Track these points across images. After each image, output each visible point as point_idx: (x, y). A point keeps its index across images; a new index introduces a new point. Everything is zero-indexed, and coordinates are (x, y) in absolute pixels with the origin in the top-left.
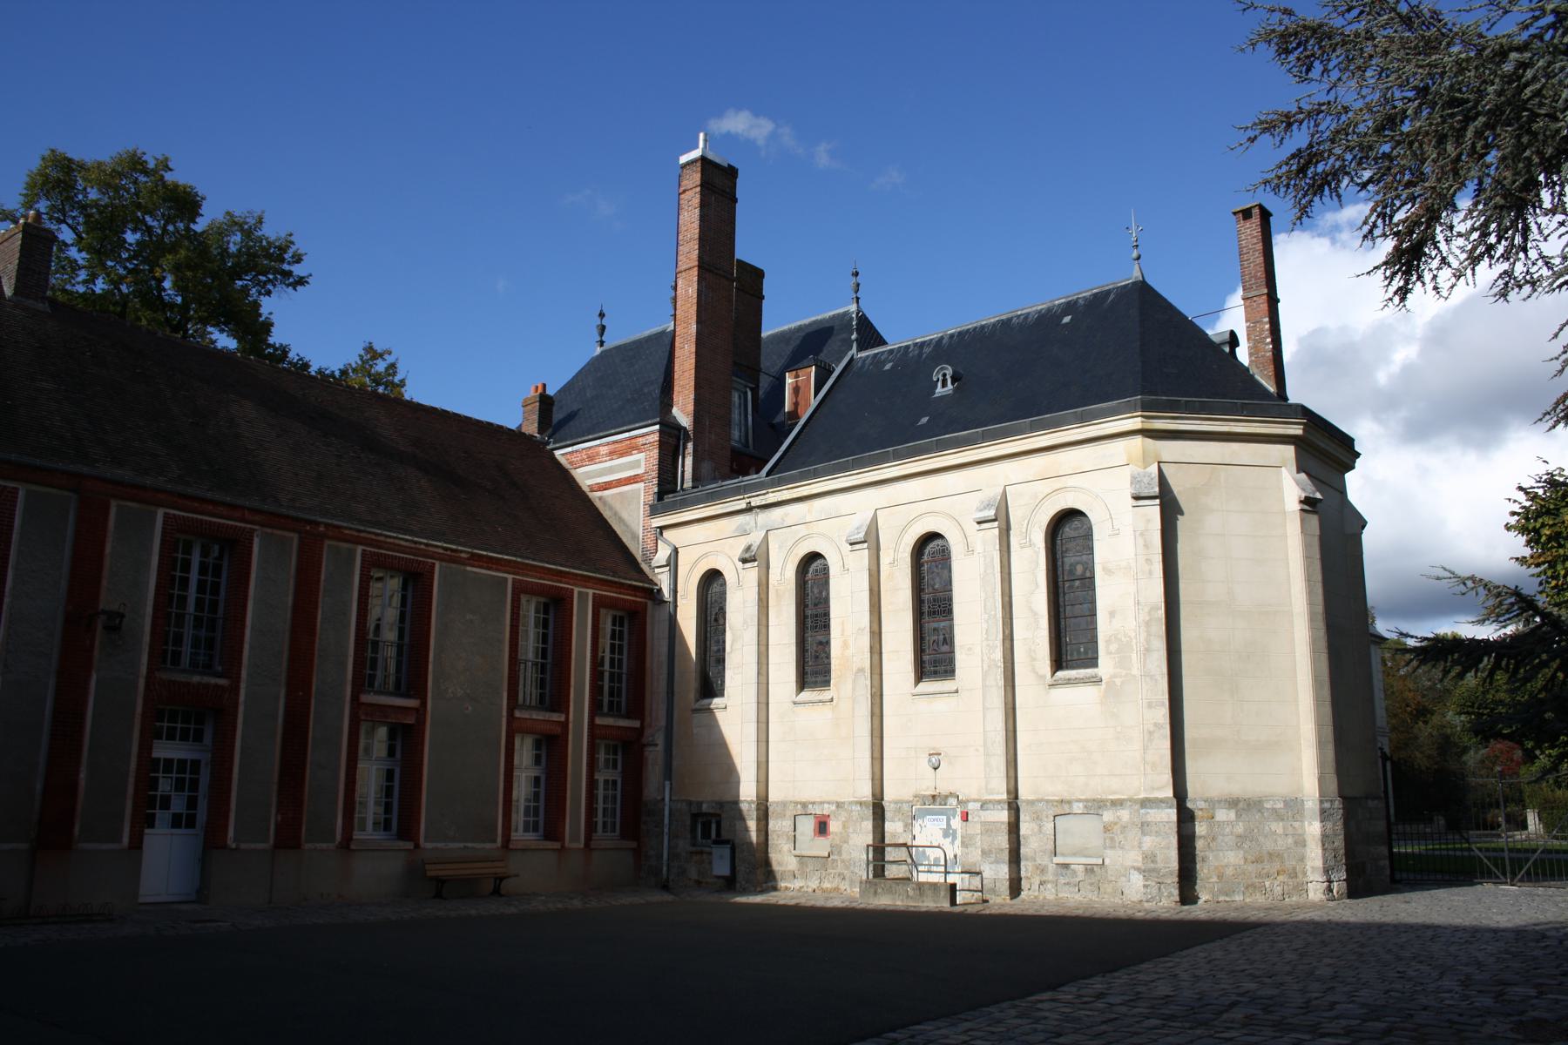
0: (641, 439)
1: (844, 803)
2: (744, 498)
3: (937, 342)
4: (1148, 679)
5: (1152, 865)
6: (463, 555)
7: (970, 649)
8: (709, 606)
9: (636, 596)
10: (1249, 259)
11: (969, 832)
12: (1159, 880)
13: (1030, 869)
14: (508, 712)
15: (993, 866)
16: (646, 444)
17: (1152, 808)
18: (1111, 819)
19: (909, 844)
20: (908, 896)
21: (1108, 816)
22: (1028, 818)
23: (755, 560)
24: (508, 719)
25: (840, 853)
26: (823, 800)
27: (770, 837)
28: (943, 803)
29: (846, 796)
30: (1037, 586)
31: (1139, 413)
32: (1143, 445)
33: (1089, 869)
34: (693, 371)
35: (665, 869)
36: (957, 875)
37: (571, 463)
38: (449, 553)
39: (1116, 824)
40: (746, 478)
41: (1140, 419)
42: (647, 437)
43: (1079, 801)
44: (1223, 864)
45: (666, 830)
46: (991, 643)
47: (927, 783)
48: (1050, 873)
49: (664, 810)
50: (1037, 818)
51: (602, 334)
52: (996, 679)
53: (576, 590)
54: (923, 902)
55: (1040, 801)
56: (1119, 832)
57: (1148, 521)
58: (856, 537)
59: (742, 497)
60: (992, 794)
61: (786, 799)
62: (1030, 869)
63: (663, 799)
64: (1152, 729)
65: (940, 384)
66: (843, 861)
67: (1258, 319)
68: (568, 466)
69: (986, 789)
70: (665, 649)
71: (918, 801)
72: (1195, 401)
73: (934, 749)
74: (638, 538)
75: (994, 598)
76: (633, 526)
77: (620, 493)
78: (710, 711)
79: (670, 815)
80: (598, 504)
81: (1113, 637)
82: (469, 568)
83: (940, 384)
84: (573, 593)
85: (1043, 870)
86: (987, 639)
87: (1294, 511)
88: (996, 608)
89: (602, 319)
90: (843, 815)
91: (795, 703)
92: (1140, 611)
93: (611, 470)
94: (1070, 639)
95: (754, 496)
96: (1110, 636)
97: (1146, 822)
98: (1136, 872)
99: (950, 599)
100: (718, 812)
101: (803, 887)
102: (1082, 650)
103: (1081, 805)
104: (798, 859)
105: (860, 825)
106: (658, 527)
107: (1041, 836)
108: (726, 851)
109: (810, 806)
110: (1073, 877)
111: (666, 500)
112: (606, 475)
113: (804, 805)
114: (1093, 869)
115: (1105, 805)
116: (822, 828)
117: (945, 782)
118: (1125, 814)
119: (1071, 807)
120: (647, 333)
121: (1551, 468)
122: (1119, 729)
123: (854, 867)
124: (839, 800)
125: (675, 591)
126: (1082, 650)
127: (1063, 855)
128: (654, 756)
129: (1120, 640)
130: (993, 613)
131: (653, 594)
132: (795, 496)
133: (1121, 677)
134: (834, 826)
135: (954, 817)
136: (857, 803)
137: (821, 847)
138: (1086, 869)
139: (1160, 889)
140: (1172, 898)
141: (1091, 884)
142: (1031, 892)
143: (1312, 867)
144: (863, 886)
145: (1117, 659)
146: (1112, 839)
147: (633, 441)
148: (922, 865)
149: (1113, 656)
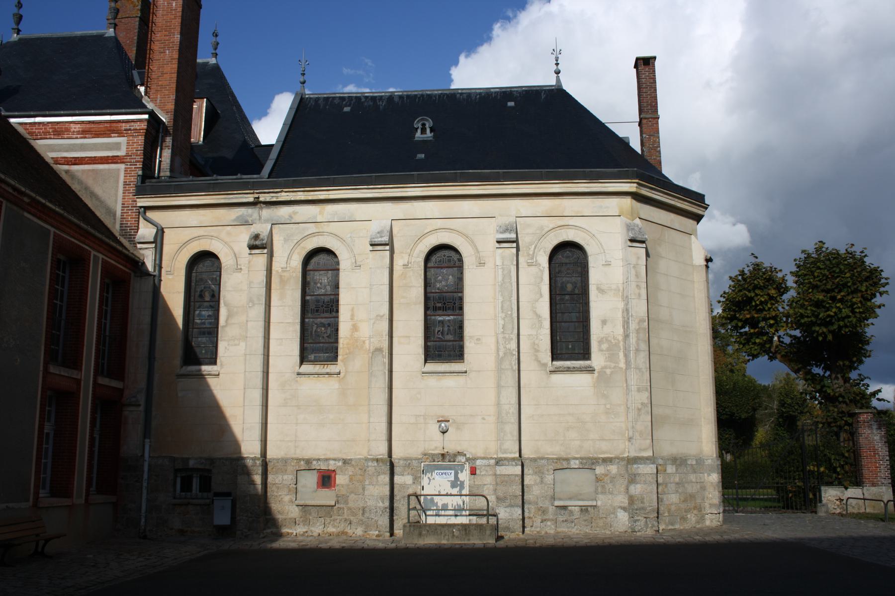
0: (124, 125)
1: (351, 460)
2: (253, 193)
3: (388, 99)
4: (638, 371)
5: (642, 505)
6: (26, 199)
7: (478, 339)
8: (193, 284)
9: (125, 266)
10: (647, 92)
11: (476, 483)
12: (646, 516)
13: (533, 511)
14: (44, 367)
15: (508, 510)
16: (130, 130)
17: (641, 464)
18: (603, 472)
19: (419, 493)
20: (453, 535)
21: (599, 470)
22: (531, 471)
23: (265, 248)
24: (43, 374)
25: (346, 502)
26: (328, 457)
27: (268, 489)
28: (452, 460)
29: (358, 452)
30: (541, 296)
31: (637, 181)
32: (631, 204)
33: (584, 510)
34: (175, 75)
35: (143, 520)
36: (465, 517)
37: (30, 133)
38: (15, 194)
39: (606, 475)
40: (219, 177)
41: (635, 185)
42: (132, 124)
43: (576, 459)
44: (670, 503)
45: (145, 484)
46: (507, 336)
47: (435, 443)
48: (550, 513)
49: (143, 465)
50: (539, 472)
51: (18, 23)
52: (511, 364)
53: (93, 253)
54: (469, 540)
55: (542, 458)
56: (609, 482)
57: (638, 258)
58: (380, 239)
59: (252, 191)
60: (505, 453)
61: (288, 456)
62: (533, 511)
63: (143, 456)
64: (640, 407)
65: (419, 131)
66: (350, 509)
67: (652, 133)
68: (27, 136)
69: (501, 449)
70: (147, 319)
71: (427, 458)
72: (661, 180)
73: (442, 417)
74: (115, 215)
75: (511, 301)
76: (110, 202)
77: (93, 170)
78: (201, 376)
79: (149, 470)
80: (64, 176)
81: (604, 339)
82: (26, 214)
83: (419, 131)
84: (90, 255)
85: (544, 511)
86: (503, 333)
87: (700, 266)
88: (512, 308)
89: (19, 9)
90: (350, 470)
91: (299, 374)
92: (633, 322)
93: (83, 148)
94: (560, 338)
95: (265, 193)
96: (602, 338)
97: (638, 474)
98: (622, 511)
99: (461, 299)
100: (207, 467)
101: (306, 532)
102: (570, 346)
103: (577, 462)
104: (301, 507)
105: (377, 479)
106: (141, 207)
107: (543, 485)
108: (228, 503)
109: (315, 462)
110: (570, 516)
111: (147, 184)
112: (75, 151)
113: (308, 461)
114: (587, 509)
115: (599, 462)
116: (326, 479)
117: (452, 443)
118: (613, 469)
119: (569, 464)
120: (79, 33)
121: (758, 261)
122: (608, 406)
123: (370, 513)
124: (345, 457)
125: (159, 265)
126: (570, 346)
127: (560, 499)
128: (133, 416)
129: (611, 341)
130: (509, 313)
131: (137, 265)
132: (310, 198)
133: (610, 368)
134: (341, 479)
135: (462, 472)
136: (373, 460)
137: (326, 497)
138: (582, 509)
139: (646, 522)
140: (654, 528)
141: (585, 520)
142: (533, 529)
143: (710, 504)
144: (407, 529)
145: (607, 355)
146: (603, 487)
147: (115, 125)
148: (430, 510)
149: (605, 352)
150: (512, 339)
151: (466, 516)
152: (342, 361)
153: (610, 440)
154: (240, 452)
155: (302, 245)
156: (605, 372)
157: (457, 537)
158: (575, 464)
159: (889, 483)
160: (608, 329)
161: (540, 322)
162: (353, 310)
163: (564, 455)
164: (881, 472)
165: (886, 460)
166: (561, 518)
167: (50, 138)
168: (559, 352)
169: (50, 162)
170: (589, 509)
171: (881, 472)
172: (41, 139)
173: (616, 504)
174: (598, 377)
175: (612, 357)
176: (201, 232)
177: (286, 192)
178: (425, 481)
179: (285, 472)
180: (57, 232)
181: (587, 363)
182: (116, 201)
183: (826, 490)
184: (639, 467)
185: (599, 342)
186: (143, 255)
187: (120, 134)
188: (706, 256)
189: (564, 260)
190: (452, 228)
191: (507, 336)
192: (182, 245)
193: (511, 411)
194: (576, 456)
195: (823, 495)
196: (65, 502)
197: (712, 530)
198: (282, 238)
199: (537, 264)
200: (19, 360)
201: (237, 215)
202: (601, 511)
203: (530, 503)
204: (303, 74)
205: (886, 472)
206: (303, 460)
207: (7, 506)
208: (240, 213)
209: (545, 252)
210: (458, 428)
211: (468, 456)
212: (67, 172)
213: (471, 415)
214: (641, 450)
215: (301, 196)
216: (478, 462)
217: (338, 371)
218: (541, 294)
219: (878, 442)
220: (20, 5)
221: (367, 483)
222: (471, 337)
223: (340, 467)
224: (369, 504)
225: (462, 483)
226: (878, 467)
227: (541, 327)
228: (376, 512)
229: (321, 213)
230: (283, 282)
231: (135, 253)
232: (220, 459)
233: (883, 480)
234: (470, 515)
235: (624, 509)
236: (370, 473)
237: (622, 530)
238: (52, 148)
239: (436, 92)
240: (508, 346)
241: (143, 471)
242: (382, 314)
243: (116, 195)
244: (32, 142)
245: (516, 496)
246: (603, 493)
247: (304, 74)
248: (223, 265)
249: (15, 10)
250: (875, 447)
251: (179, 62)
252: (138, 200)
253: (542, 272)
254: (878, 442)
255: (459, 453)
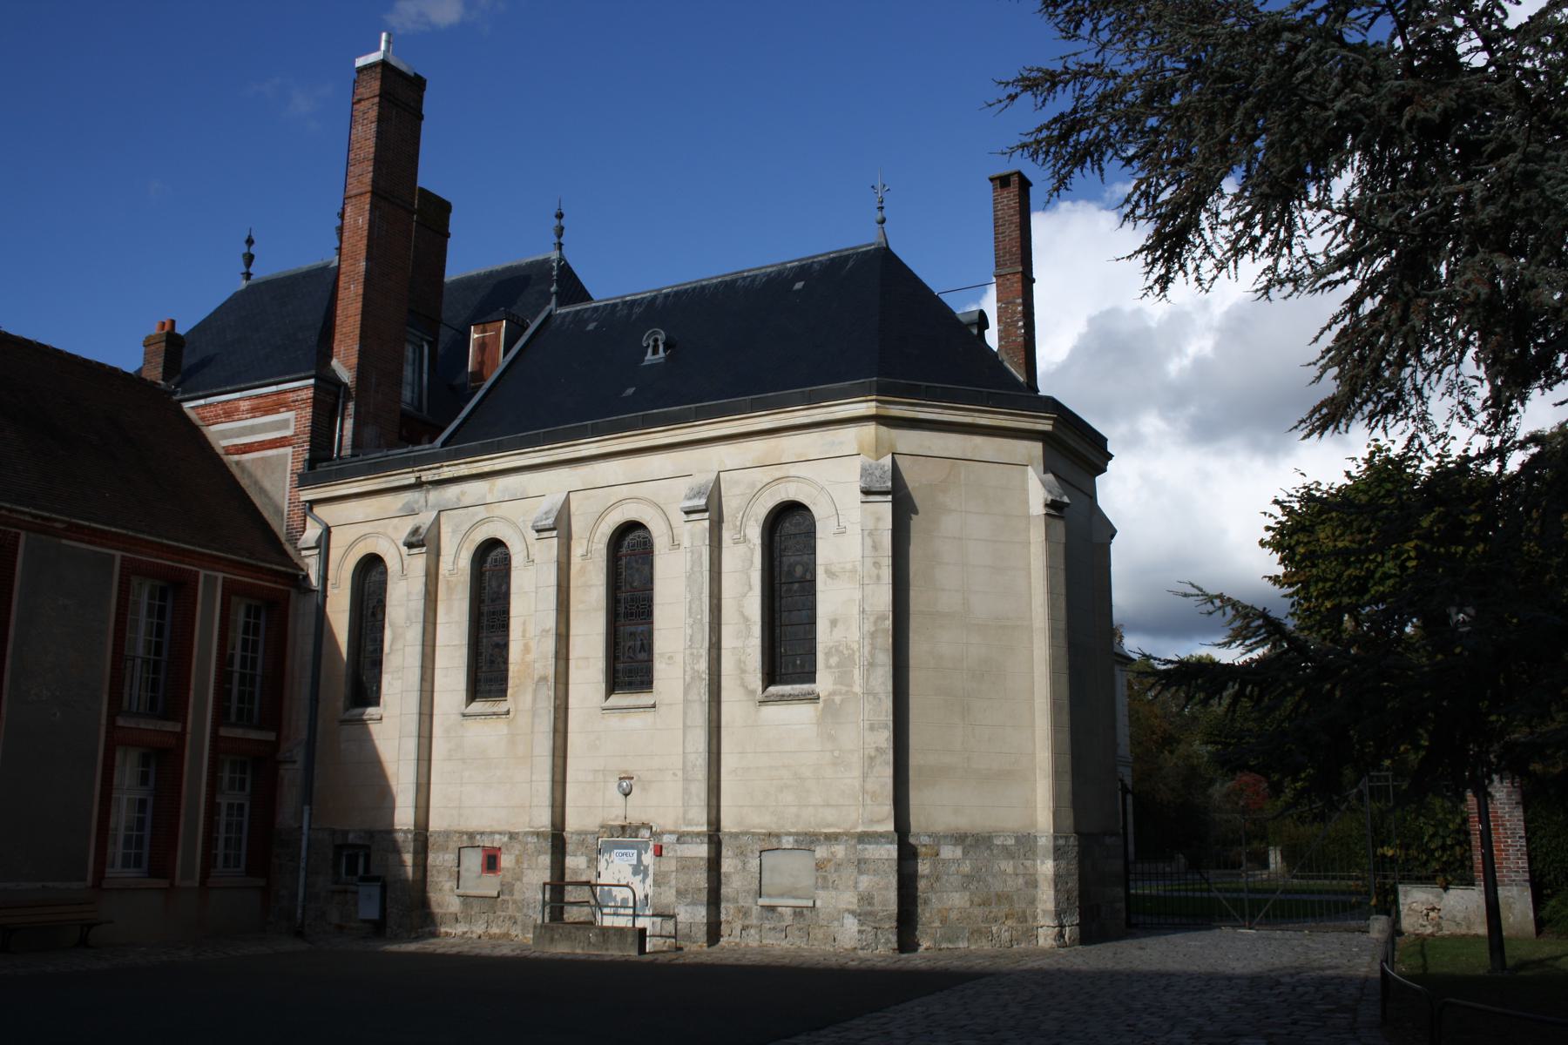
0: (291, 395)
1: (517, 833)
2: (413, 472)
3: (649, 302)
4: (871, 698)
5: (869, 908)
6: (57, 525)
7: (670, 658)
8: (366, 598)
9: (275, 582)
11: (662, 869)
12: (877, 925)
13: (732, 911)
17: (870, 843)
18: (825, 855)
19: (593, 882)
21: (821, 852)
23: (423, 546)
25: (511, 893)
31: (874, 397)
32: (877, 434)
33: (798, 912)
34: (359, 318)
35: (299, 911)
37: (203, 419)
39: (830, 860)
41: (874, 404)
42: (300, 393)
43: (789, 834)
45: (303, 865)
47: (614, 810)
48: (753, 916)
49: (301, 840)
50: (741, 854)
52: (699, 694)
53: (202, 573)
57: (878, 519)
58: (544, 523)
59: (411, 470)
60: (689, 824)
62: (732, 911)
63: (301, 827)
64: (873, 754)
65: (650, 351)
66: (515, 902)
67: (1010, 299)
68: (199, 423)
69: (684, 818)
73: (625, 772)
76: (277, 498)
77: (262, 458)
78: (362, 723)
79: (309, 846)
80: (235, 470)
82: (64, 542)
83: (650, 351)
85: (746, 913)
86: (690, 647)
88: (702, 610)
93: (253, 430)
95: (425, 470)
96: (831, 648)
98: (850, 916)
103: (791, 839)
106: (307, 501)
108: (375, 890)
109: (478, 837)
111: (319, 470)
113: (471, 835)
115: (818, 840)
116: (491, 862)
117: (638, 809)
118: (840, 850)
119: (780, 841)
122: (836, 753)
125: (324, 578)
126: (798, 662)
127: (769, 896)
128: (291, 775)
129: (842, 652)
131: (297, 579)
132: (474, 471)
133: (840, 694)
134: (506, 861)
135: (646, 852)
137: (489, 885)
138: (795, 912)
141: (800, 930)
142: (731, 939)
143: (1043, 911)
144: (538, 931)
147: (282, 396)
150: (701, 656)
151: (649, 916)
152: (512, 695)
153: (837, 805)
154: (392, 824)
155: (471, 537)
156: (833, 700)
157: (594, 945)
158: (788, 842)
159: (1525, 881)
160: (838, 634)
161: (748, 628)
162: (524, 623)
163: (774, 829)
164: (1509, 859)
165: (1520, 837)
166: (767, 925)
167: (222, 422)
168: (790, 671)
169: (220, 451)
170: (805, 911)
171: (1509, 859)
172: (213, 424)
173: (843, 906)
174: (823, 709)
175: (843, 677)
176: (366, 528)
177: (447, 466)
178: (602, 866)
179: (445, 849)
180: (125, 554)
181: (806, 687)
182: (284, 497)
183: (1406, 892)
184: (866, 849)
185: (826, 654)
186: (307, 565)
187: (288, 406)
188: (1046, 500)
189: (793, 530)
190: (640, 495)
191: (695, 651)
192: (345, 549)
193: (698, 763)
194: (792, 830)
195: (1401, 899)
196: (163, 883)
197: (1044, 953)
198: (450, 530)
199: (745, 540)
200: (58, 714)
201: (404, 502)
202: (820, 915)
203: (728, 901)
204: (881, 208)
205: (1519, 859)
206: (467, 833)
207: (43, 886)
208: (407, 499)
209: (756, 521)
210: (644, 789)
211: (654, 829)
212: (238, 463)
213: (660, 770)
214: (872, 822)
215: (463, 470)
216: (666, 839)
217: (506, 710)
218: (750, 586)
219: (1504, 804)
220: (250, 242)
221: (525, 866)
222: (662, 655)
223: (506, 844)
224: (527, 895)
225: (646, 868)
226: (1503, 850)
227: (749, 635)
228: (535, 907)
229: (491, 490)
230: (450, 590)
231: (299, 562)
232: (380, 832)
233: (1513, 874)
234: (653, 915)
235: (853, 913)
236: (529, 851)
237: (848, 947)
238: (224, 435)
239: (715, 281)
240: (696, 667)
241: (300, 848)
242: (548, 628)
243: (284, 487)
244: (206, 430)
245: (700, 890)
246: (825, 888)
247: (882, 208)
248: (389, 571)
249: (245, 250)
250: (1497, 812)
251: (364, 298)
252: (301, 493)
253: (752, 551)
254: (1504, 804)
255: (644, 825)
